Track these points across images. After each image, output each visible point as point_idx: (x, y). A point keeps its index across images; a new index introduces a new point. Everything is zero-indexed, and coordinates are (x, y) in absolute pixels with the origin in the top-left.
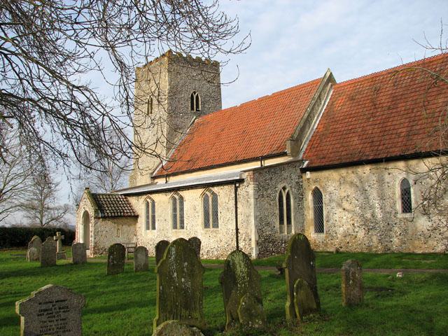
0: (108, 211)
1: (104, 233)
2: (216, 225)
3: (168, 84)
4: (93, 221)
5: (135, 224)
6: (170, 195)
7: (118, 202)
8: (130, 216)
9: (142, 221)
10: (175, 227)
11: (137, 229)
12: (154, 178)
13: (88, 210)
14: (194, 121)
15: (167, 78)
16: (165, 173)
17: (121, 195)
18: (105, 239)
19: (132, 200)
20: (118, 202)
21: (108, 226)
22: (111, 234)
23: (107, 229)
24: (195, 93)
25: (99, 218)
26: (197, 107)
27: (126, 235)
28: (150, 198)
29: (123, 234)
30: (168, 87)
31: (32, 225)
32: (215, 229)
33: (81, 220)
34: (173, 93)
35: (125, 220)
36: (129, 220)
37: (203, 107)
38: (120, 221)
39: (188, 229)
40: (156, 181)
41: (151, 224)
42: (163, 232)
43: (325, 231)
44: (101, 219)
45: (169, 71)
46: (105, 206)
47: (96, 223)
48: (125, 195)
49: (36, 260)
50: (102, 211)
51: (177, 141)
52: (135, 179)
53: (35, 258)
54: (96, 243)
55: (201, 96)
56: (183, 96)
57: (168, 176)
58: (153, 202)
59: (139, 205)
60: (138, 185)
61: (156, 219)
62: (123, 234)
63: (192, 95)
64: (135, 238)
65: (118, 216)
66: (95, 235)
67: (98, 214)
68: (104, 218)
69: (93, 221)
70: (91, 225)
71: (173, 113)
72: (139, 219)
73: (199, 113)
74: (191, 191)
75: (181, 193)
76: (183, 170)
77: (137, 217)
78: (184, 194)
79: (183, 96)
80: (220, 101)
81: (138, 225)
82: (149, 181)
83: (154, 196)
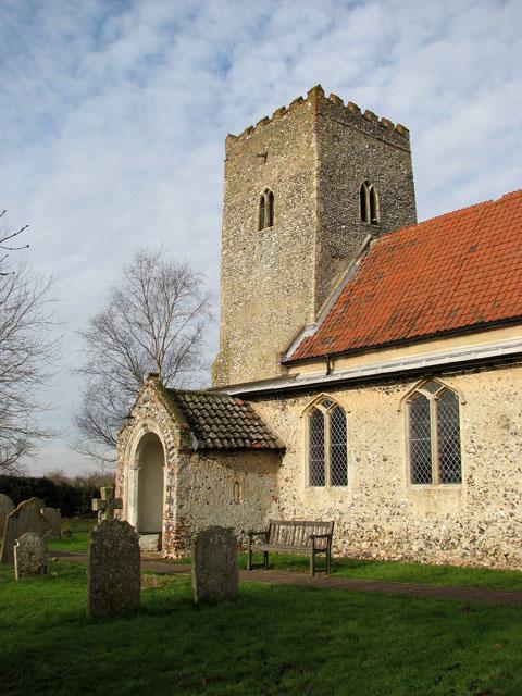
0: (211, 435)
1: (203, 491)
2: (340, 478)
3: (316, 156)
4: (172, 459)
5: (275, 471)
6: (400, 393)
7: (230, 412)
8: (267, 450)
9: (297, 462)
10: (421, 474)
11: (281, 483)
12: (288, 365)
13: (157, 431)
14: (369, 243)
15: (314, 144)
16: (325, 350)
17: (233, 396)
18: (206, 509)
19: (267, 411)
20: (230, 412)
21: (213, 472)
22: (222, 498)
23: (210, 482)
24: (367, 184)
25: (192, 452)
26: (373, 215)
27: (255, 496)
28: (326, 404)
29: (248, 494)
30: (317, 164)
31: (57, 477)
32: (422, 486)
33: (131, 457)
34: (328, 174)
35: (251, 460)
36: (261, 460)
37: (384, 217)
38: (241, 460)
39: (477, 480)
40: (293, 371)
41: (331, 465)
42: (375, 492)
43: (464, 479)
44: (196, 456)
45: (317, 130)
46: (203, 422)
47: (183, 466)
48: (243, 397)
49: (38, 572)
50: (199, 434)
51: (338, 282)
52: (227, 372)
53: (35, 568)
54: (181, 519)
55: (379, 193)
56: (346, 186)
57: (332, 357)
58: (339, 416)
59: (289, 423)
60: (232, 383)
61: (351, 457)
62: (248, 494)
63: (362, 188)
64: (275, 505)
65: (239, 449)
66: (180, 498)
67: (190, 440)
68: (205, 452)
69: (172, 459)
70: (166, 470)
71: (328, 226)
72: (287, 460)
73: (377, 229)
74: (487, 378)
75: (448, 382)
76: (381, 341)
77: (277, 453)
78: (460, 384)
79: (346, 186)
80: (414, 208)
81: (284, 472)
82: (274, 370)
83: (343, 398)
